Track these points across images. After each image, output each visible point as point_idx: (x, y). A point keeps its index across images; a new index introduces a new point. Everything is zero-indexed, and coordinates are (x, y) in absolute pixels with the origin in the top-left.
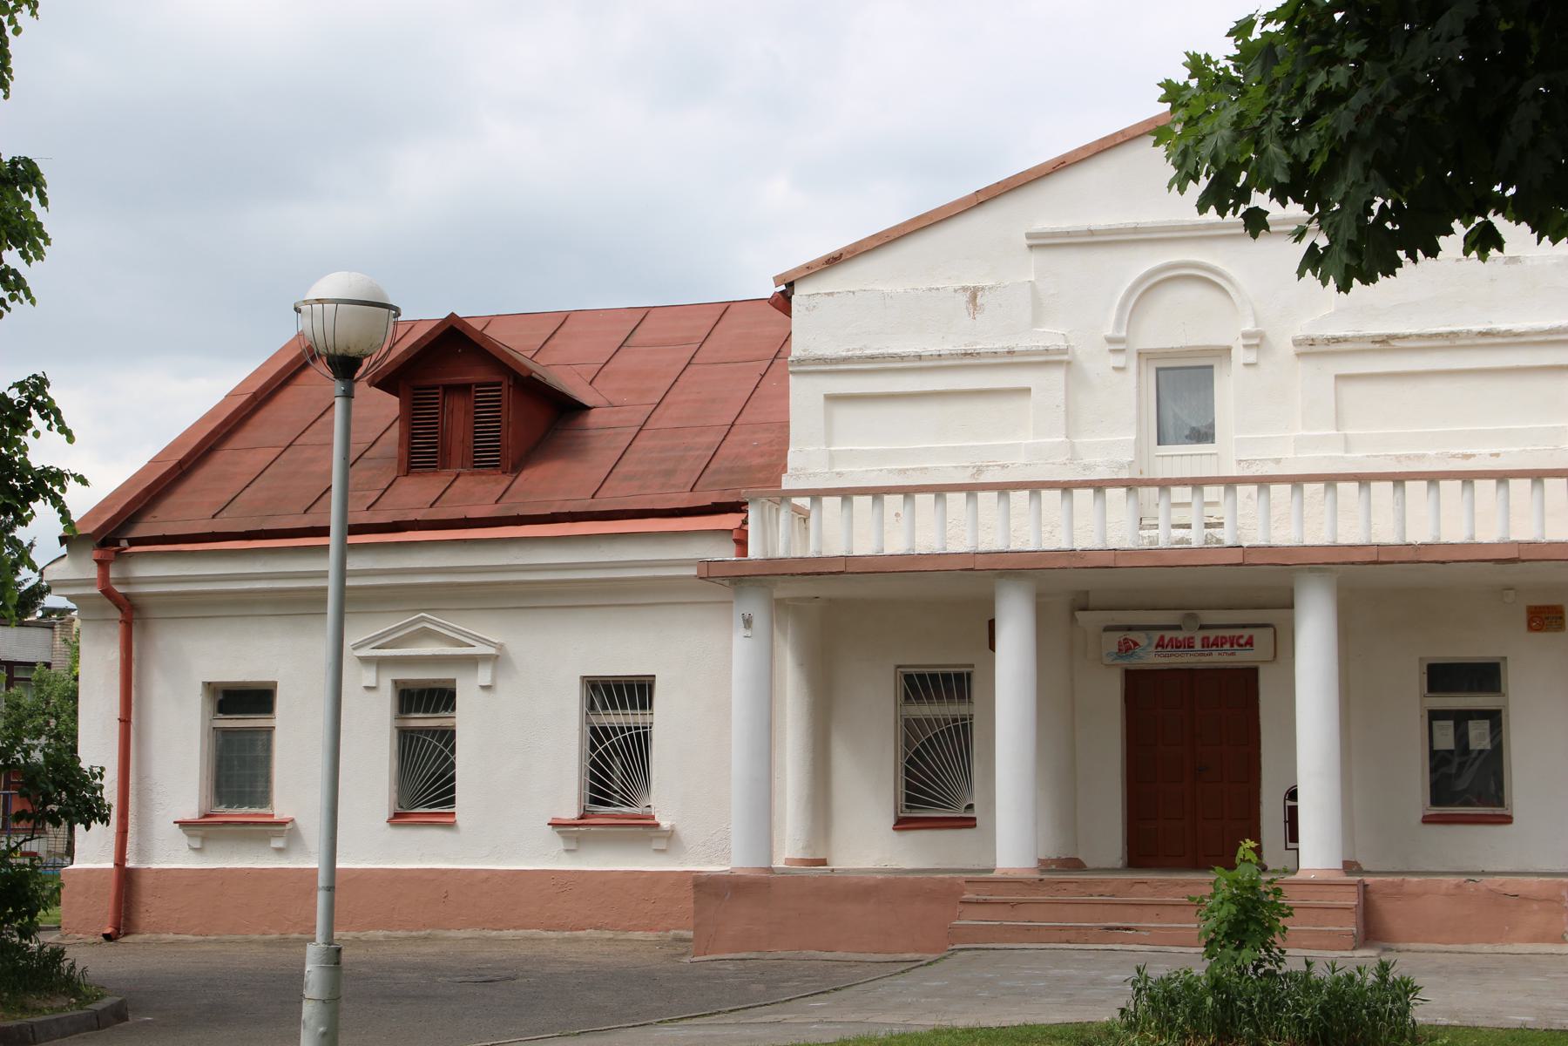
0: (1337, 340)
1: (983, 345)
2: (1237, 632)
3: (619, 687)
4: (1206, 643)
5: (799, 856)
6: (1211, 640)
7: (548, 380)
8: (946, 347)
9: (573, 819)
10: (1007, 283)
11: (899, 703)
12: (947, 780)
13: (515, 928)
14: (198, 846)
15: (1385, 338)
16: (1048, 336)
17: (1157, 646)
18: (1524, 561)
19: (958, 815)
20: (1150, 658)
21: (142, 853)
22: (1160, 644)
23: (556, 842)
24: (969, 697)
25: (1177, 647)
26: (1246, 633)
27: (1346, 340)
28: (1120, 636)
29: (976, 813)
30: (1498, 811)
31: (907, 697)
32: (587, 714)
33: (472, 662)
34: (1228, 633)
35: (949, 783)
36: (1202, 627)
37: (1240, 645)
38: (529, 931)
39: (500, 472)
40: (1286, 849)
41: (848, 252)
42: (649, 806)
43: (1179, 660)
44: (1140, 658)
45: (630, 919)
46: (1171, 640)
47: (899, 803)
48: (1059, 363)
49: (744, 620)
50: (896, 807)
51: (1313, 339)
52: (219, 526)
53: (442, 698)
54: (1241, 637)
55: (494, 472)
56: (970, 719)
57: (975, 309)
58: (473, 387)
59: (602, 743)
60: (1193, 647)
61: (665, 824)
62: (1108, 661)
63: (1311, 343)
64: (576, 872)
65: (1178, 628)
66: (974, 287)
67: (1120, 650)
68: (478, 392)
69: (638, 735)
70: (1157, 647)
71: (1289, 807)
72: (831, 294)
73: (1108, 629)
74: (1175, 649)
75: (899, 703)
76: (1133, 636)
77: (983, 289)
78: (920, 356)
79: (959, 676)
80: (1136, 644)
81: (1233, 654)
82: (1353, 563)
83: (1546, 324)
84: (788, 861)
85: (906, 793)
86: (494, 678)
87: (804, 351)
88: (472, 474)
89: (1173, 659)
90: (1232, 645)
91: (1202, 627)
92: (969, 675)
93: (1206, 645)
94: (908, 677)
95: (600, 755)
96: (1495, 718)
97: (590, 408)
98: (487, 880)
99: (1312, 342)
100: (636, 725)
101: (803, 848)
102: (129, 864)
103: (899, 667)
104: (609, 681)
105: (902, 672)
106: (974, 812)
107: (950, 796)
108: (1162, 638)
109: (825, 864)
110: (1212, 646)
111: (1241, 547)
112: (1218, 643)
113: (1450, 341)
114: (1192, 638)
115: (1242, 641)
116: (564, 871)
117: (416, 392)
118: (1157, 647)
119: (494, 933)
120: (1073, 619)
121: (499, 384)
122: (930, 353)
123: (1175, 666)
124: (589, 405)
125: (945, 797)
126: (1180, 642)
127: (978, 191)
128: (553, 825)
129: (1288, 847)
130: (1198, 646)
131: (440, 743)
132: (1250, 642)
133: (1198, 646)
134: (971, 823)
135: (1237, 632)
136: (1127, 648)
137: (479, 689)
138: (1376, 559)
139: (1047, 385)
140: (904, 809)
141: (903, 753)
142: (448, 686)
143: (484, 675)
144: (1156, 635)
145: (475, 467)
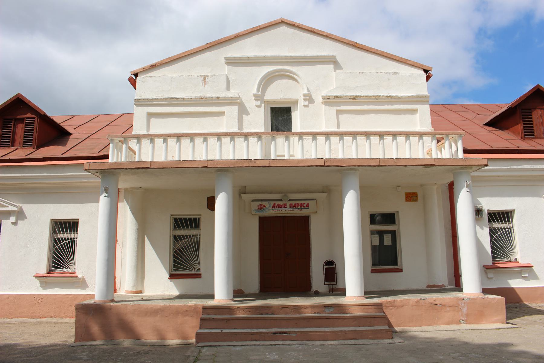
0: (337, 97)
1: (208, 95)
2: (303, 202)
3: (65, 223)
4: (291, 206)
5: (131, 290)
6: (293, 205)
8: (194, 96)
9: (44, 274)
10: (217, 74)
11: (172, 229)
12: (191, 260)
13: (18, 317)
16: (232, 93)
17: (273, 207)
18: (436, 166)
19: (194, 273)
20: (270, 212)
22: (274, 206)
23: (37, 282)
24: (199, 227)
25: (280, 207)
26: (306, 202)
27: (341, 97)
28: (258, 203)
29: (202, 272)
30: (396, 267)
31: (175, 227)
32: (52, 233)
34: (299, 202)
35: (190, 259)
36: (290, 200)
38: (23, 319)
39: (32, 148)
40: (325, 285)
41: (159, 63)
42: (75, 269)
43: (281, 212)
44: (266, 212)
45: (65, 313)
46: (278, 205)
47: (171, 268)
49: (104, 189)
50: (170, 270)
51: (329, 96)
55: (30, 148)
56: (199, 236)
57: (205, 83)
58: (25, 119)
59: (57, 244)
60: (286, 207)
61: (80, 276)
62: (253, 213)
63: (328, 97)
64: (44, 295)
65: (281, 200)
66: (205, 75)
67: (258, 209)
69: (72, 241)
70: (272, 208)
71: (325, 268)
72: (151, 77)
73: (253, 201)
74: (279, 208)
75: (172, 229)
76: (263, 203)
77: (208, 76)
78: (184, 99)
79: (195, 219)
80: (264, 206)
81: (302, 210)
82: (370, 166)
83: (409, 95)
84: (126, 292)
85: (174, 264)
87: (140, 97)
88: (22, 149)
89: (279, 212)
90: (301, 207)
91: (290, 200)
92: (199, 219)
93: (291, 206)
94: (175, 220)
95: (56, 249)
96: (393, 234)
97: (72, 134)
98: (8, 298)
99: (328, 97)
100: (71, 238)
101: (132, 287)
103: (172, 215)
104: (62, 221)
105: (173, 217)
106: (200, 272)
107: (190, 262)
108: (274, 204)
109: (141, 293)
110: (293, 207)
111: (323, 159)
112: (296, 206)
113: (376, 99)
114: (286, 204)
115: (305, 205)
116: (39, 295)
118: (272, 208)
119: (9, 320)
120: (240, 197)
121: (34, 118)
122: (188, 97)
124: (72, 133)
125: (192, 264)
126: (281, 205)
127: (207, 44)
128: (36, 277)
129: (325, 284)
130: (288, 207)
131: (61, 243)
132: (308, 206)
133: (288, 207)
134: (199, 276)
135: (303, 202)
136: (261, 208)
137: (11, 223)
139: (232, 111)
140: (173, 270)
141: (173, 249)
144: (272, 203)
145: (23, 146)
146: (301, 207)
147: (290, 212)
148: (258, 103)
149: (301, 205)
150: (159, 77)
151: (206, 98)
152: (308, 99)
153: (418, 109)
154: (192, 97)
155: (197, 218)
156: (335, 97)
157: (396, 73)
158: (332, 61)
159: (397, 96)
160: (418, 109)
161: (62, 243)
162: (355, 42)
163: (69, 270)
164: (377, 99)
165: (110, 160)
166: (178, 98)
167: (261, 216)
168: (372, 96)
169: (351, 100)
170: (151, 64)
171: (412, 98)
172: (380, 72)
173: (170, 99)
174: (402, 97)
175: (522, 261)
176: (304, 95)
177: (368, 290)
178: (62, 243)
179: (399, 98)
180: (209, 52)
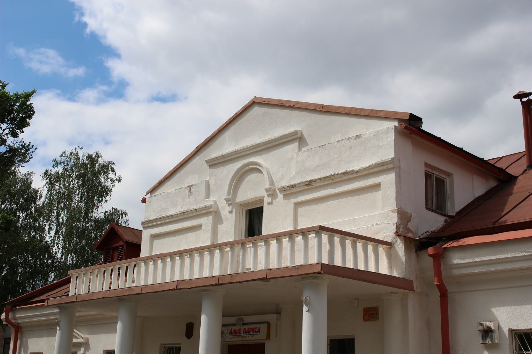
15: (309, 182)
25: (236, 334)
26: (258, 326)
36: (244, 324)
37: (256, 332)
43: (236, 339)
51: (284, 188)
54: (256, 328)
60: (240, 333)
63: (284, 189)
65: (234, 325)
68: (120, 249)
81: (253, 336)
83: (367, 165)
90: (253, 333)
115: (256, 330)
117: (108, 252)
118: (229, 334)
123: (246, 342)
132: (259, 331)
138: (217, 283)
139: (207, 221)
142: (264, 343)
144: (229, 328)
146: (253, 333)
147: (244, 339)
148: (230, 208)
149: (253, 330)
150: (160, 195)
151: (187, 212)
152: (272, 194)
153: (202, 224)
154: (178, 213)
155: (177, 348)
156: (290, 188)
157: (358, 136)
159: (353, 170)
160: (202, 224)
162: (322, 105)
164: (333, 180)
165: (70, 295)
166: (168, 216)
167: (230, 344)
168: (326, 177)
169: (307, 187)
170: (158, 181)
171: (372, 168)
172: (341, 140)
173: (164, 218)
174: (359, 170)
176: (267, 190)
179: (357, 172)
180: (198, 157)
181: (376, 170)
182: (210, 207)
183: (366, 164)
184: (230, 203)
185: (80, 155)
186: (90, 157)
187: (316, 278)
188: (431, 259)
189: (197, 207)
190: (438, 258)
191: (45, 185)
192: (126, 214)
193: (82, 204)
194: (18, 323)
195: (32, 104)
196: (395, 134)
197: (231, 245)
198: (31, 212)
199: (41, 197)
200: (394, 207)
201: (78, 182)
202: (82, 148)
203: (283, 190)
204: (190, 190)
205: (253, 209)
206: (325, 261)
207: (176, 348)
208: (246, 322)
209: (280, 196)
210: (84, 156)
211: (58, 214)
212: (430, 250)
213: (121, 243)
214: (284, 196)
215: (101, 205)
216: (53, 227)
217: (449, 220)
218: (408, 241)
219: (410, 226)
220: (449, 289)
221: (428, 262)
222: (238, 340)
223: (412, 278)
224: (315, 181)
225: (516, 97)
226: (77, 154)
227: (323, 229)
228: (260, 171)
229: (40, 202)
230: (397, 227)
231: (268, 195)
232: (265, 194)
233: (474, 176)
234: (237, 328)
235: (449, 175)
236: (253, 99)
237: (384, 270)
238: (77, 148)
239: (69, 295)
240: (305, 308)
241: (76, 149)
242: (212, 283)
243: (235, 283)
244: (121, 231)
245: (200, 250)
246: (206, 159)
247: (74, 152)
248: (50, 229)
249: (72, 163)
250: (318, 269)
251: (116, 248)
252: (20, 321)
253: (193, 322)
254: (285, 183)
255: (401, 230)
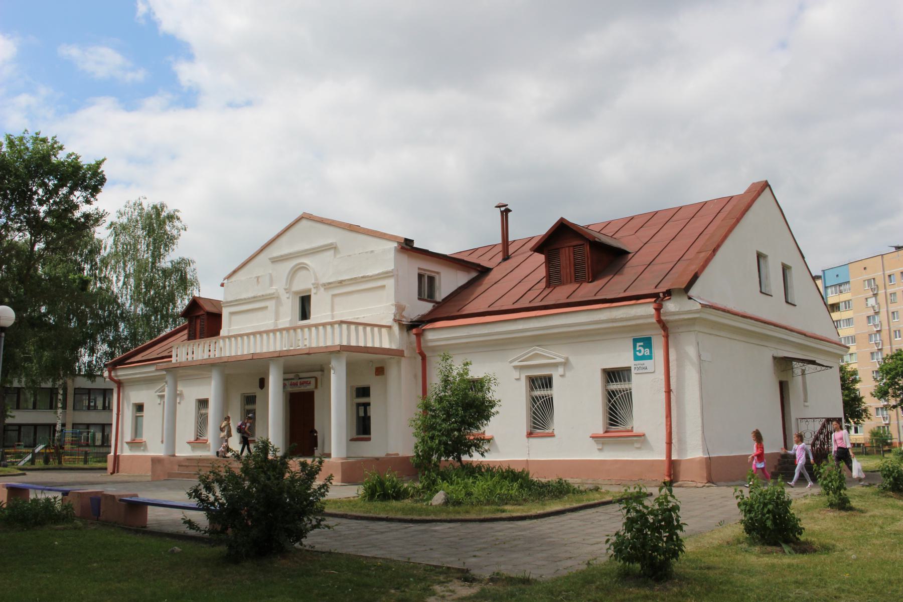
7: (602, 240)
14: (600, 448)
21: (681, 450)
23: (189, 446)
26: (309, 380)
33: (556, 365)
36: (300, 379)
48: (274, 298)
52: (629, 293)
53: (547, 382)
59: (613, 398)
69: (549, 398)
86: (564, 371)
97: (492, 269)
102: (674, 458)
113: (354, 281)
123: (302, 391)
128: (188, 443)
132: (310, 383)
137: (515, 381)
139: (271, 304)
143: (561, 370)
144: (290, 381)
147: (300, 389)
148: (288, 295)
149: (306, 383)
158: (332, 247)
161: (540, 401)
163: (204, 438)
165: (174, 360)
169: (339, 284)
175: (636, 431)
176: (313, 284)
177: (348, 456)
178: (540, 401)
179: (371, 276)
181: (382, 276)
182: (273, 294)
183: (377, 272)
184: (287, 291)
185: (145, 206)
186: (155, 207)
187: (337, 353)
188: (415, 336)
189: (263, 293)
190: (419, 335)
191: (109, 236)
192: (193, 262)
193: (379, 564)
194: (119, 380)
195: (103, 171)
196: (395, 250)
197: (287, 329)
198: (96, 264)
199: (105, 248)
200: (394, 302)
201: (143, 233)
202: (145, 198)
203: (324, 285)
204: (258, 279)
205: (305, 296)
206: (345, 343)
207: (253, 396)
208: (300, 377)
209: (322, 289)
210: (148, 206)
211: (125, 265)
212: (414, 331)
213: (202, 312)
214: (325, 289)
215: (168, 254)
216: (120, 278)
217: (436, 305)
218: (401, 325)
219: (404, 314)
220: (428, 354)
221: (414, 338)
222: (296, 389)
223: (404, 348)
224: (345, 281)
225: (496, 207)
226: (141, 204)
227: (342, 322)
228: (307, 269)
229: (104, 253)
230: (394, 315)
231: (314, 288)
232: (312, 287)
233: (458, 271)
234: (295, 381)
235: (438, 273)
236: (302, 214)
237: (386, 345)
238: (141, 198)
239: (171, 361)
240: (332, 372)
241: (139, 199)
242: (275, 355)
243: (290, 356)
244: (202, 303)
245: (267, 332)
246: (271, 256)
247: (138, 202)
248: (118, 280)
249: (136, 214)
250: (339, 349)
251: (198, 316)
252: (121, 378)
253: (263, 390)
254: (325, 280)
255: (398, 317)
